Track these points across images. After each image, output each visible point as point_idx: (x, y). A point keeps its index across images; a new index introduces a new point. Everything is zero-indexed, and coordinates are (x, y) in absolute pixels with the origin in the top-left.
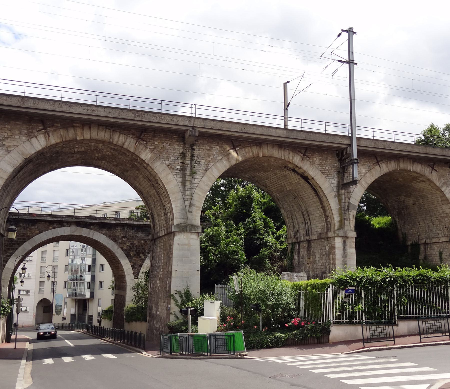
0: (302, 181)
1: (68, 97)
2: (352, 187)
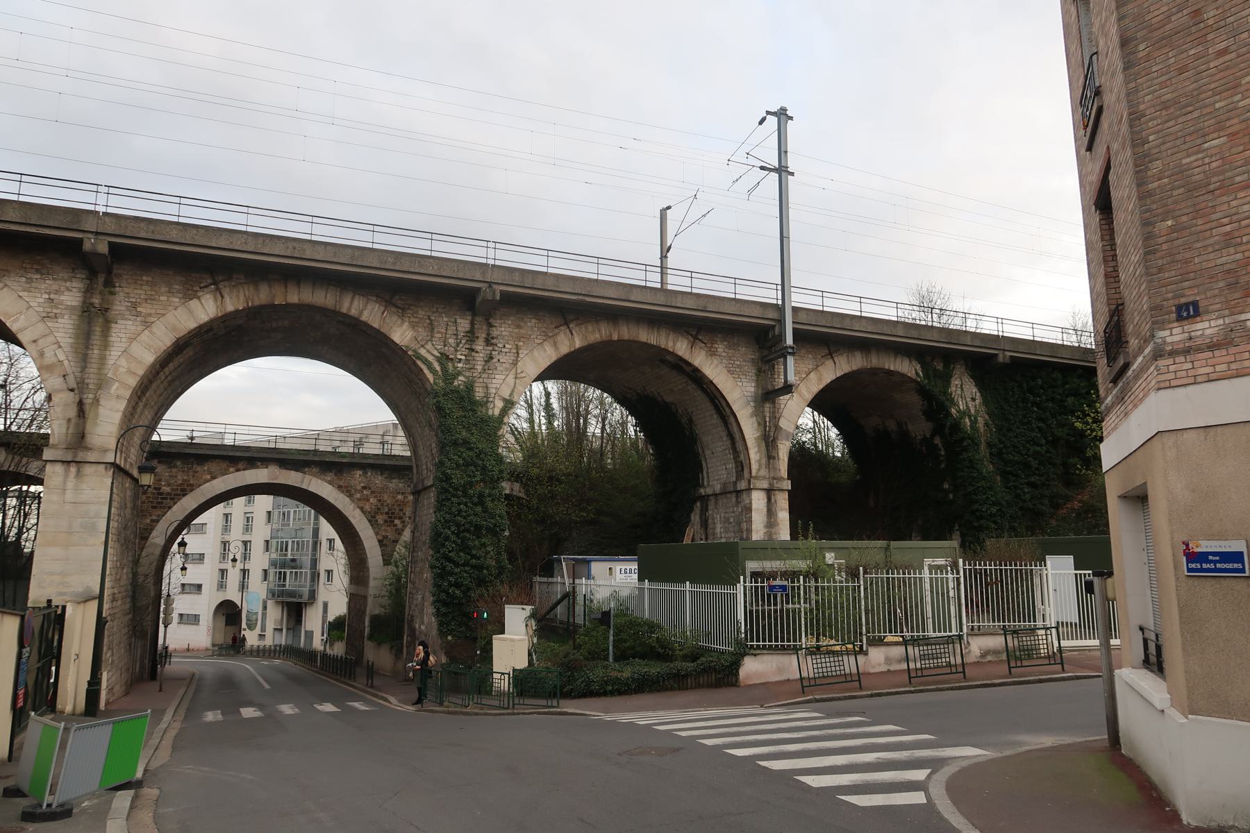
0: (692, 387)
1: (1053, 337)
2: (783, 399)
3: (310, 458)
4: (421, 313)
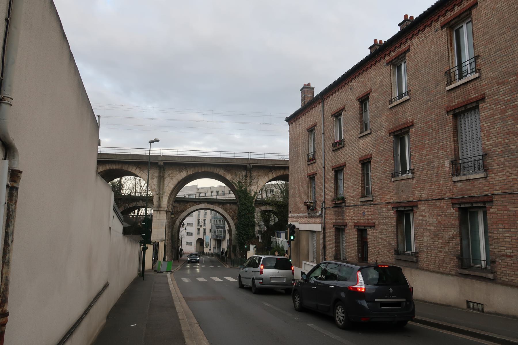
3: (215, 201)
4: (233, 171)
